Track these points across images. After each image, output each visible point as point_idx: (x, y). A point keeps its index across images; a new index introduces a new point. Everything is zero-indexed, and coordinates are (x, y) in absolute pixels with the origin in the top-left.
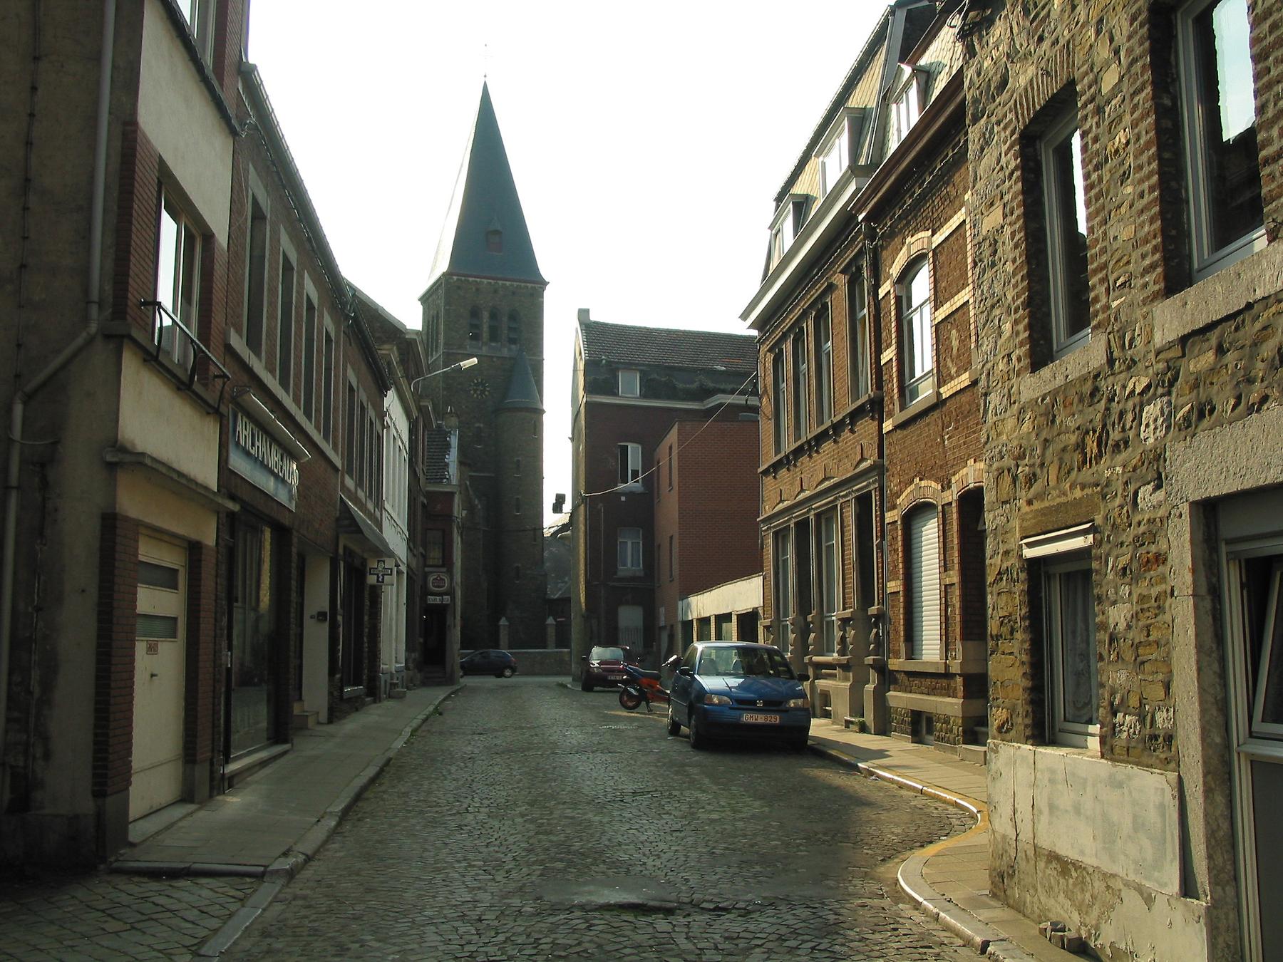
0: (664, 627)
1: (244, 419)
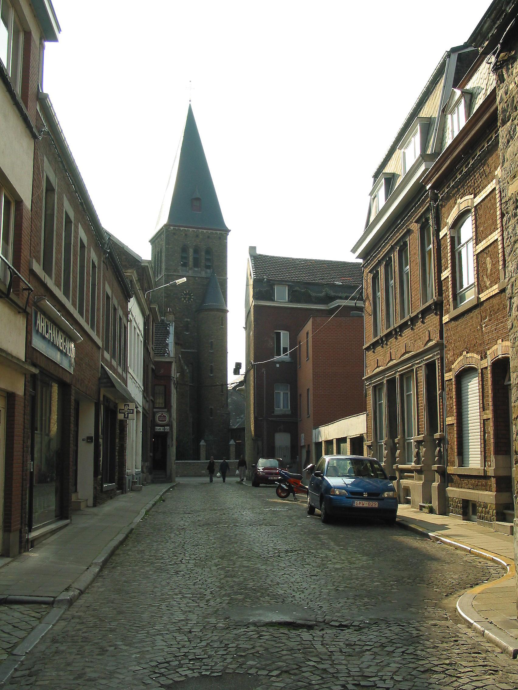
0: (304, 446)
1: (42, 316)
